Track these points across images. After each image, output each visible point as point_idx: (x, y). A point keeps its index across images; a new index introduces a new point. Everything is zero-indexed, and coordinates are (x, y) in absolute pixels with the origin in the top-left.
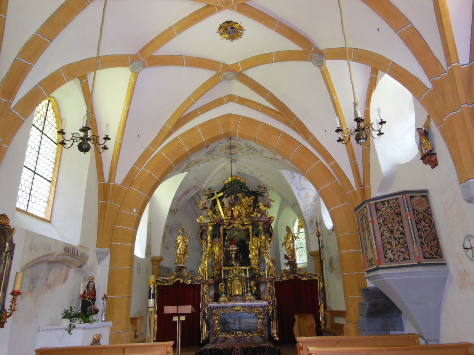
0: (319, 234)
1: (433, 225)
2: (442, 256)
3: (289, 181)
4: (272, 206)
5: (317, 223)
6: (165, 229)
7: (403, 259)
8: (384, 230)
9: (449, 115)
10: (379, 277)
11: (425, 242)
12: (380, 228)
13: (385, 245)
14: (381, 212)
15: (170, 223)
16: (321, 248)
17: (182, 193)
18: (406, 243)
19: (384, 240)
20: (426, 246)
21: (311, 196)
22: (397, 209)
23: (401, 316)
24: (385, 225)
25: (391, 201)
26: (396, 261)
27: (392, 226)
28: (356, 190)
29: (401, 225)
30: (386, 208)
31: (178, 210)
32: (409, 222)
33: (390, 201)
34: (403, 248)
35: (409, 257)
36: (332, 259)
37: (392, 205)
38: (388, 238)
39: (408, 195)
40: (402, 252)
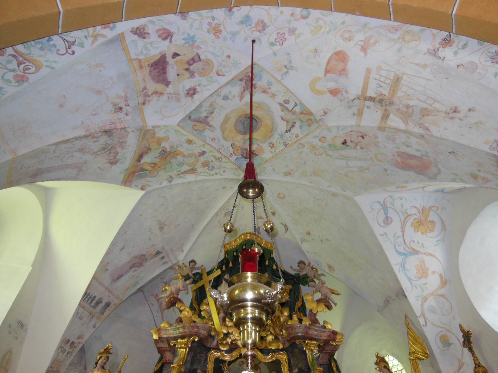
3: (378, 230)
4: (336, 305)
6: (61, 348)
15: (80, 337)
17: (124, 258)
21: (433, 273)
31: (112, 306)
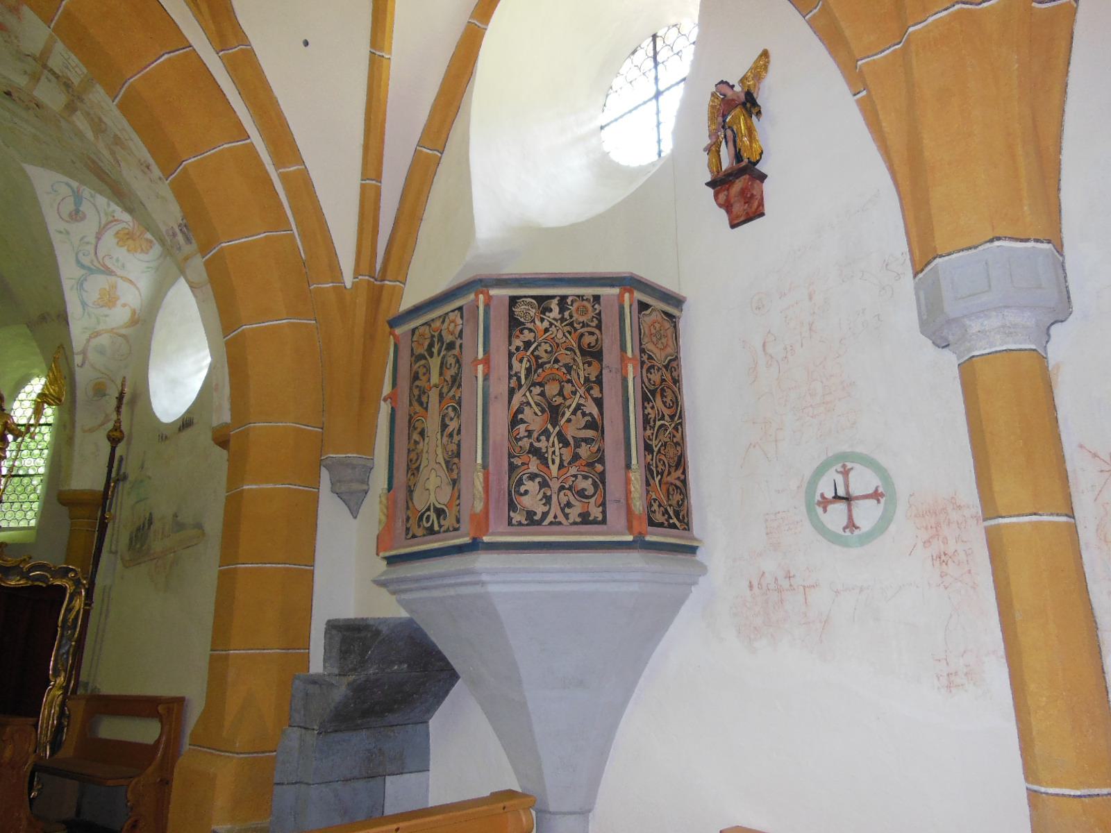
0: (117, 434)
1: (680, 417)
2: (687, 524)
3: (54, 225)
5: (120, 398)
7: (578, 520)
8: (528, 404)
9: (945, 13)
10: (467, 579)
11: (657, 467)
12: (512, 392)
13: (522, 459)
14: (528, 336)
16: (115, 477)
18: (601, 460)
19: (521, 439)
20: (657, 480)
22: (592, 334)
23: (426, 722)
24: (534, 384)
25: (572, 302)
26: (551, 523)
27: (561, 393)
28: (349, 285)
29: (595, 392)
30: (551, 324)
32: (625, 388)
33: (569, 301)
34: (586, 478)
35: (604, 512)
36: (150, 522)
37: (575, 316)
38: (535, 435)
39: (638, 296)
40: (581, 494)
